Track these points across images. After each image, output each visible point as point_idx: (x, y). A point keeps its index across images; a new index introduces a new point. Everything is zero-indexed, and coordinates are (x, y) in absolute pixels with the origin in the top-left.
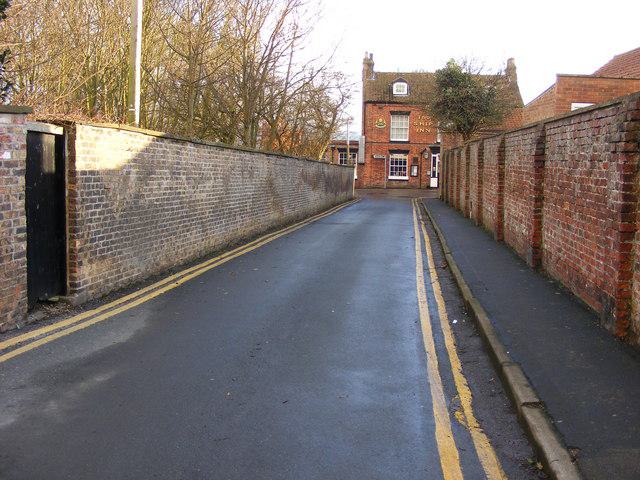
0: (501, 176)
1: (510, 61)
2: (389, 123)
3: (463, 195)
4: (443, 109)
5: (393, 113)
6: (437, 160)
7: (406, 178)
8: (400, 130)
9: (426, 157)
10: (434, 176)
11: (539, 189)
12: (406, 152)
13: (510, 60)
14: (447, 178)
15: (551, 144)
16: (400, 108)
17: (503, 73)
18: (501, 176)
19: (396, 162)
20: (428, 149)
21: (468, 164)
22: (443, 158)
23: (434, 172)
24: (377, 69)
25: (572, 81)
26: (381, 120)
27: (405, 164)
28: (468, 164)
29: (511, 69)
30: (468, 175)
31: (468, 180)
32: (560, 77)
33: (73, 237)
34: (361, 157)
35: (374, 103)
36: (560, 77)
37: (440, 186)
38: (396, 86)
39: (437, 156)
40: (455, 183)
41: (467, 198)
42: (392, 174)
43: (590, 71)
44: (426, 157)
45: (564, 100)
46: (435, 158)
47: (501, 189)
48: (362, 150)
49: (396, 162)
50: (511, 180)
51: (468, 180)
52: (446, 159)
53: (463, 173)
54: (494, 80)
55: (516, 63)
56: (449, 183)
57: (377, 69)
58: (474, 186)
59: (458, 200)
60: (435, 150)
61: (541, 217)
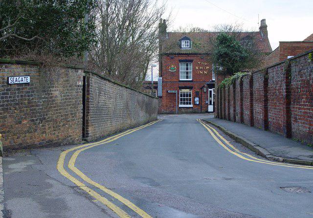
0: (252, 94)
1: (263, 21)
2: (178, 68)
3: (232, 111)
4: (222, 58)
5: (181, 61)
6: (213, 93)
7: (191, 106)
8: (185, 73)
9: (205, 91)
10: (211, 104)
11: (266, 96)
12: (190, 88)
13: (263, 21)
14: (221, 103)
15: (270, 75)
16: (187, 58)
17: (257, 30)
18: (252, 94)
19: (187, 95)
20: (206, 85)
21: (234, 91)
22: (218, 91)
23: (211, 102)
24: (170, 29)
25: (288, 45)
26: (172, 66)
27: (190, 96)
28: (234, 91)
29: (263, 27)
30: (234, 98)
31: (235, 101)
32: (281, 43)
33: (88, 115)
34: (160, 92)
35: (168, 55)
36: (281, 43)
37: (216, 110)
38: (183, 43)
39: (212, 90)
40: (227, 104)
41: (235, 111)
42: (181, 103)
43: (301, 39)
44: (205, 91)
45: (284, 55)
46: (211, 92)
47: (252, 100)
48: (160, 87)
49: (187, 95)
50: (256, 96)
51: (235, 101)
52: (219, 91)
53: (231, 97)
54: (249, 36)
55: (267, 23)
56: (223, 106)
57: (170, 29)
58: (238, 103)
59: (229, 114)
60: (211, 86)
61: (267, 108)
